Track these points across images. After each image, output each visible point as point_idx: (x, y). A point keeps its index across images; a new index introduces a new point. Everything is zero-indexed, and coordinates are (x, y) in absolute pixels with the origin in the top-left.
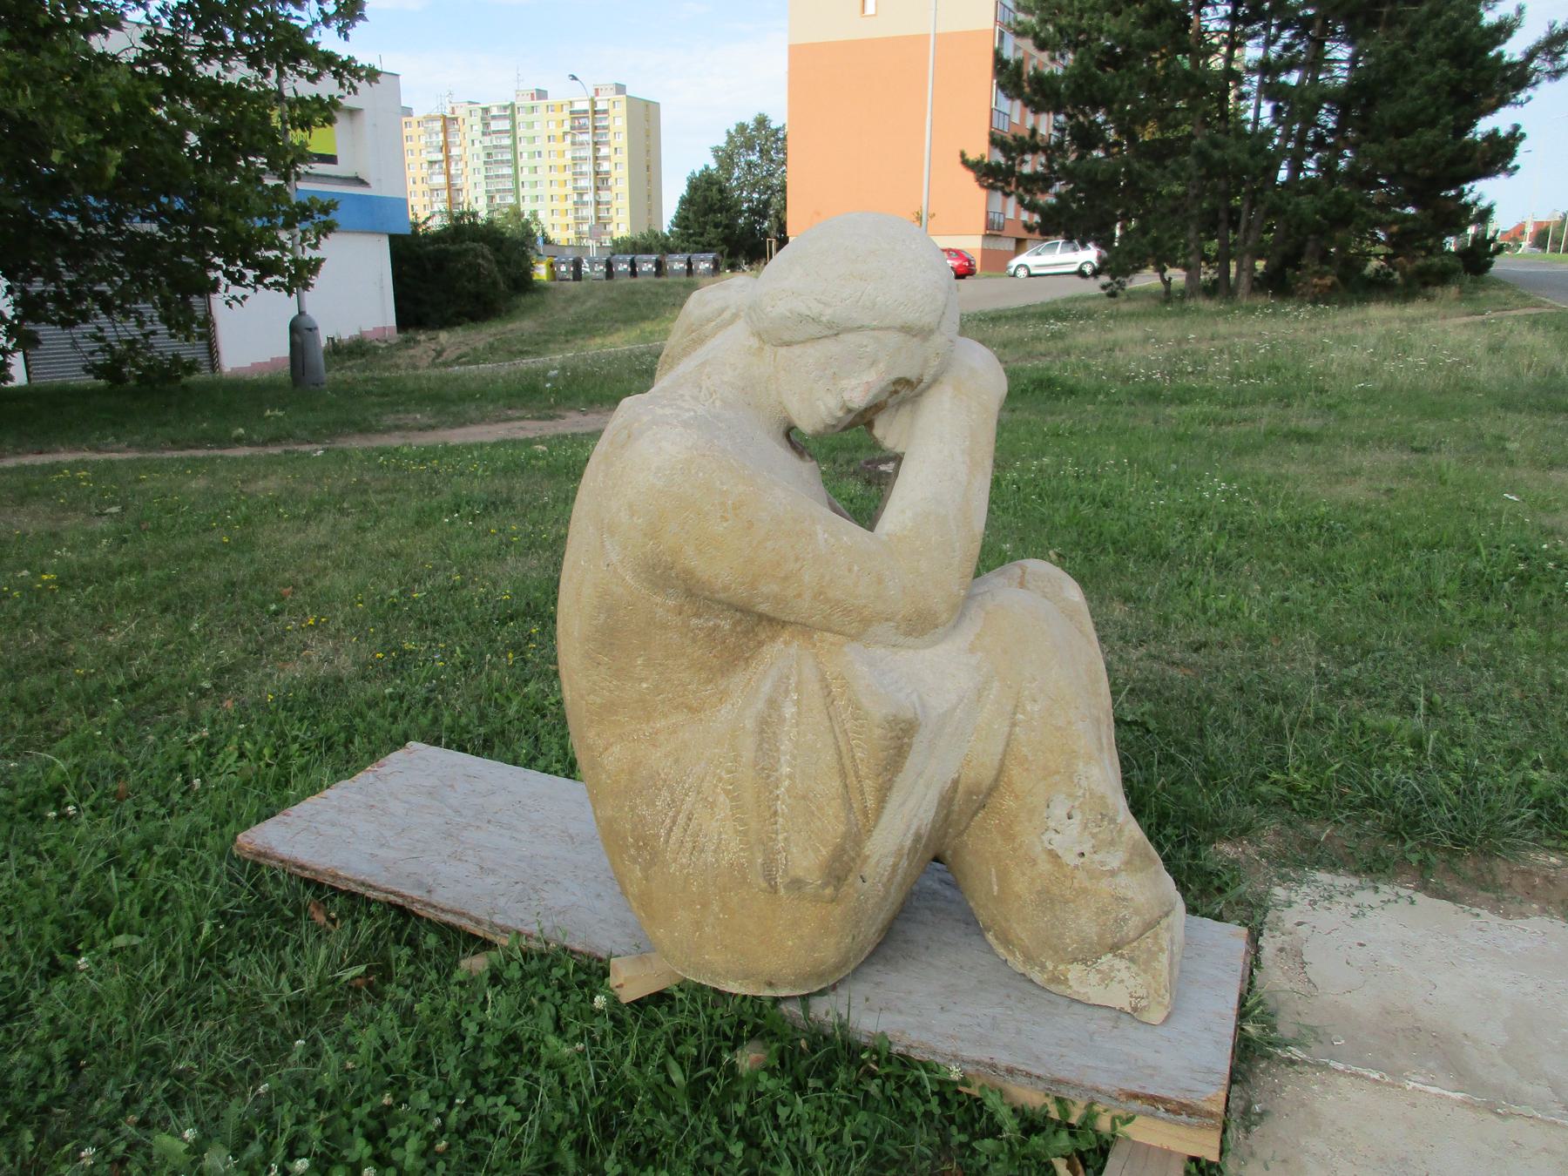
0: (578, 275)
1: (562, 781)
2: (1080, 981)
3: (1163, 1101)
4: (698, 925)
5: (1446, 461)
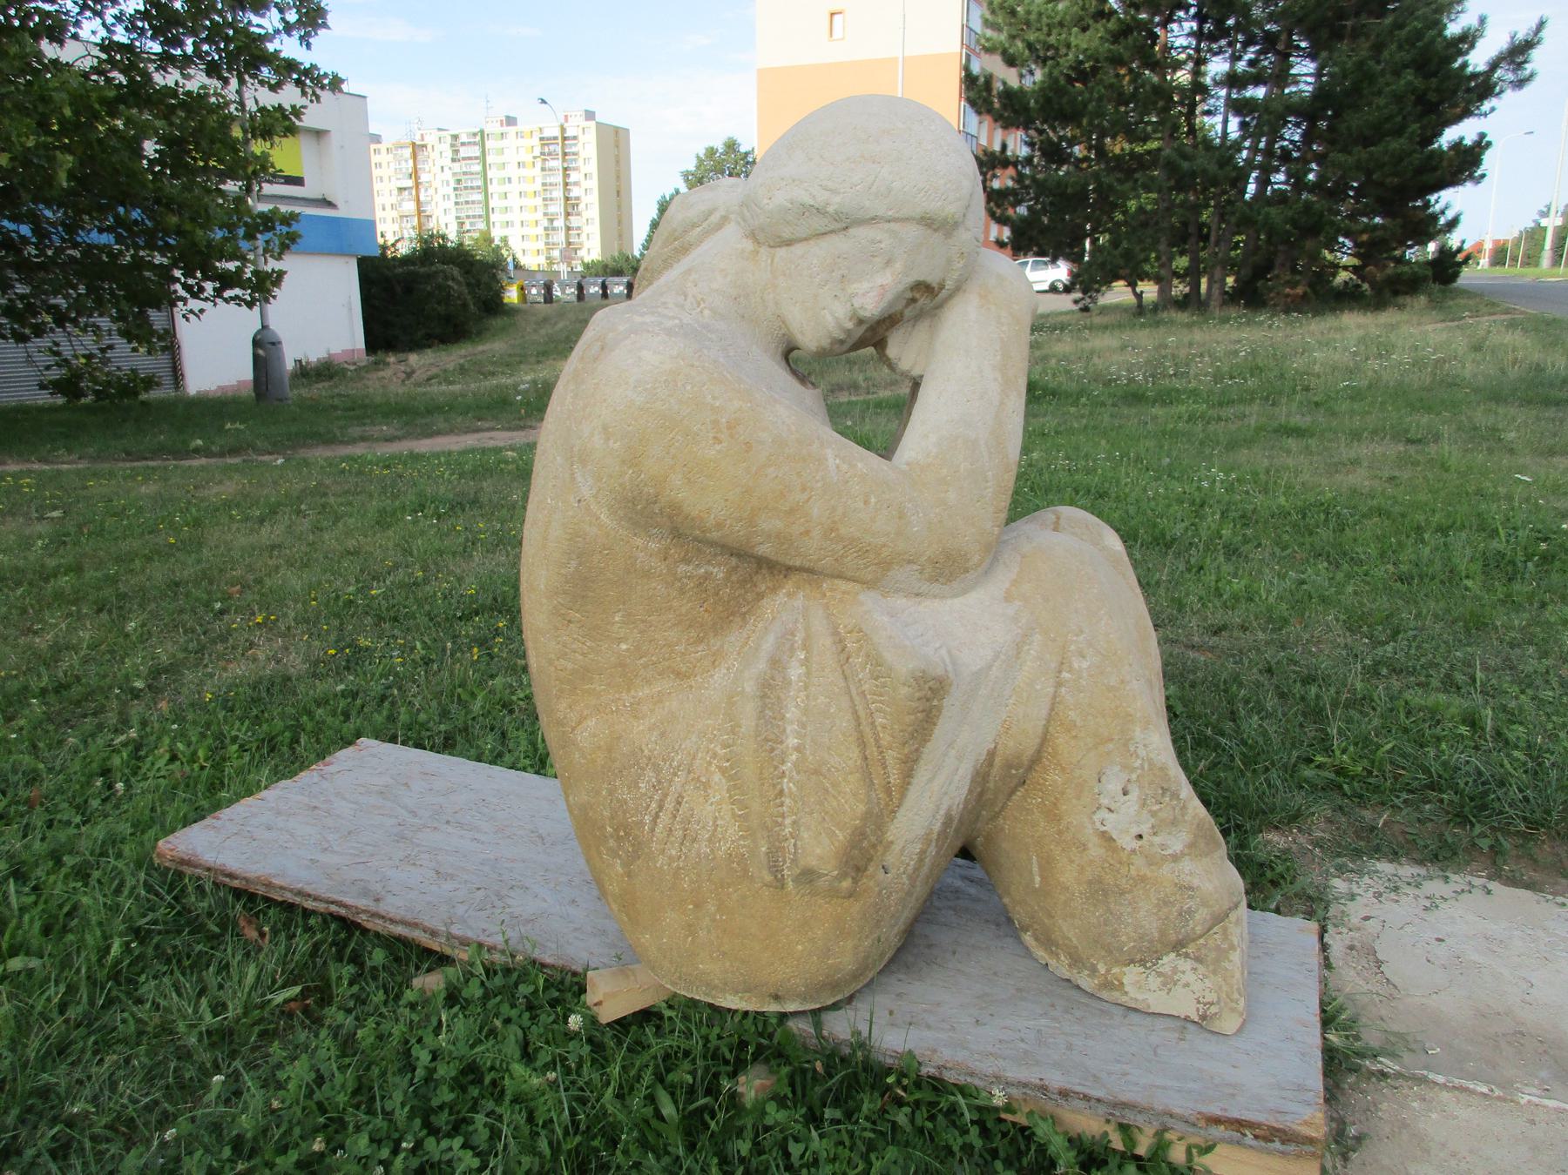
0: (549, 297)
1: (530, 777)
2: (1138, 985)
3: (1251, 1125)
4: (691, 929)
5: (1449, 450)
